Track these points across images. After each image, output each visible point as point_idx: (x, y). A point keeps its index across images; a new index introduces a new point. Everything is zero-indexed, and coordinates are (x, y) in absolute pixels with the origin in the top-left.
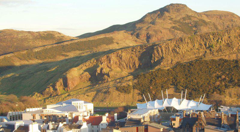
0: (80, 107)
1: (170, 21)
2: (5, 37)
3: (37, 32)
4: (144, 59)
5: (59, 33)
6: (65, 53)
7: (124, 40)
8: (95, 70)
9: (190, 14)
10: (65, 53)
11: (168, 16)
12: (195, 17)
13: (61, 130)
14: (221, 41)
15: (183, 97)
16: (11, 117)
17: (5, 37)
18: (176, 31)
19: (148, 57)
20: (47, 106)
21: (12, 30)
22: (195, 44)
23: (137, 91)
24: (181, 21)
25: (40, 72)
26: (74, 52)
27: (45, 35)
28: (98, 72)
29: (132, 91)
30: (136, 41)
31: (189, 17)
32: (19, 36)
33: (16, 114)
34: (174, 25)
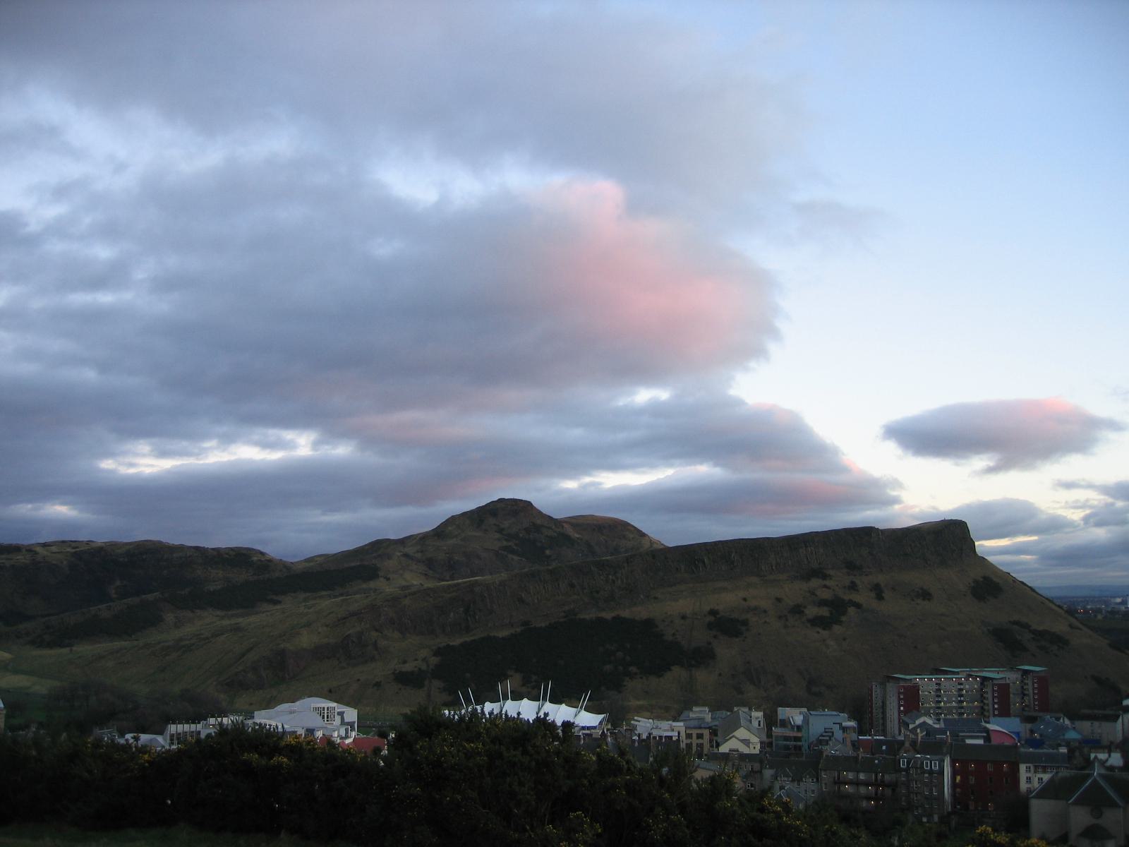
0: (328, 718)
1: (498, 536)
2: (144, 557)
3: (213, 549)
4: (452, 614)
5: (262, 554)
6: (275, 597)
7: (401, 572)
8: (347, 634)
9: (539, 522)
10: (275, 597)
11: (495, 525)
12: (550, 528)
13: (619, 748)
14: (614, 578)
15: (545, 699)
16: (172, 736)
17: (144, 557)
18: (510, 556)
19: (462, 609)
20: (255, 712)
21: (160, 542)
22: (561, 586)
23: (437, 684)
24: (521, 535)
25: (225, 636)
26: (292, 594)
27: (230, 556)
28: (1113, 805)
29: (426, 682)
30: (426, 575)
31: (538, 528)
32: (174, 555)
33: (179, 732)
34: (505, 543)
